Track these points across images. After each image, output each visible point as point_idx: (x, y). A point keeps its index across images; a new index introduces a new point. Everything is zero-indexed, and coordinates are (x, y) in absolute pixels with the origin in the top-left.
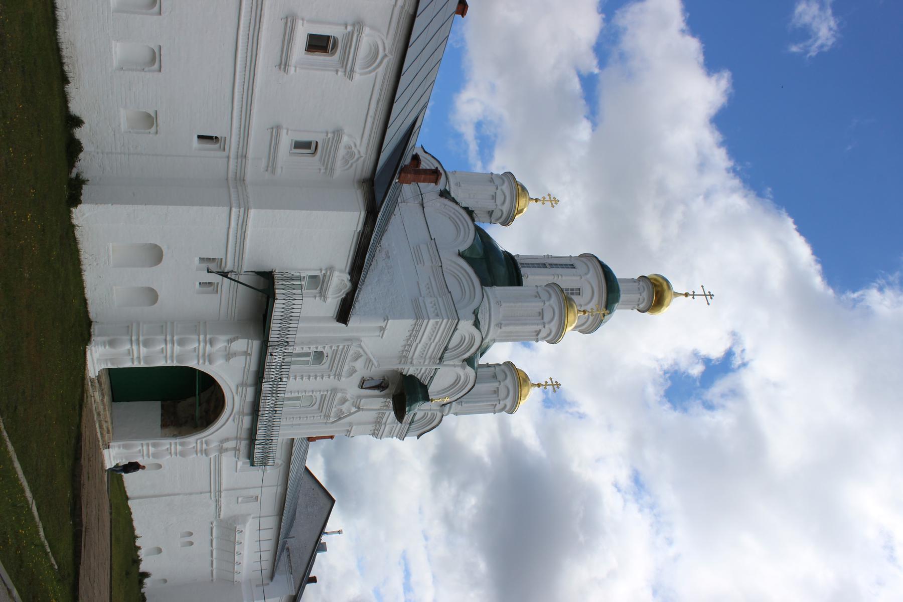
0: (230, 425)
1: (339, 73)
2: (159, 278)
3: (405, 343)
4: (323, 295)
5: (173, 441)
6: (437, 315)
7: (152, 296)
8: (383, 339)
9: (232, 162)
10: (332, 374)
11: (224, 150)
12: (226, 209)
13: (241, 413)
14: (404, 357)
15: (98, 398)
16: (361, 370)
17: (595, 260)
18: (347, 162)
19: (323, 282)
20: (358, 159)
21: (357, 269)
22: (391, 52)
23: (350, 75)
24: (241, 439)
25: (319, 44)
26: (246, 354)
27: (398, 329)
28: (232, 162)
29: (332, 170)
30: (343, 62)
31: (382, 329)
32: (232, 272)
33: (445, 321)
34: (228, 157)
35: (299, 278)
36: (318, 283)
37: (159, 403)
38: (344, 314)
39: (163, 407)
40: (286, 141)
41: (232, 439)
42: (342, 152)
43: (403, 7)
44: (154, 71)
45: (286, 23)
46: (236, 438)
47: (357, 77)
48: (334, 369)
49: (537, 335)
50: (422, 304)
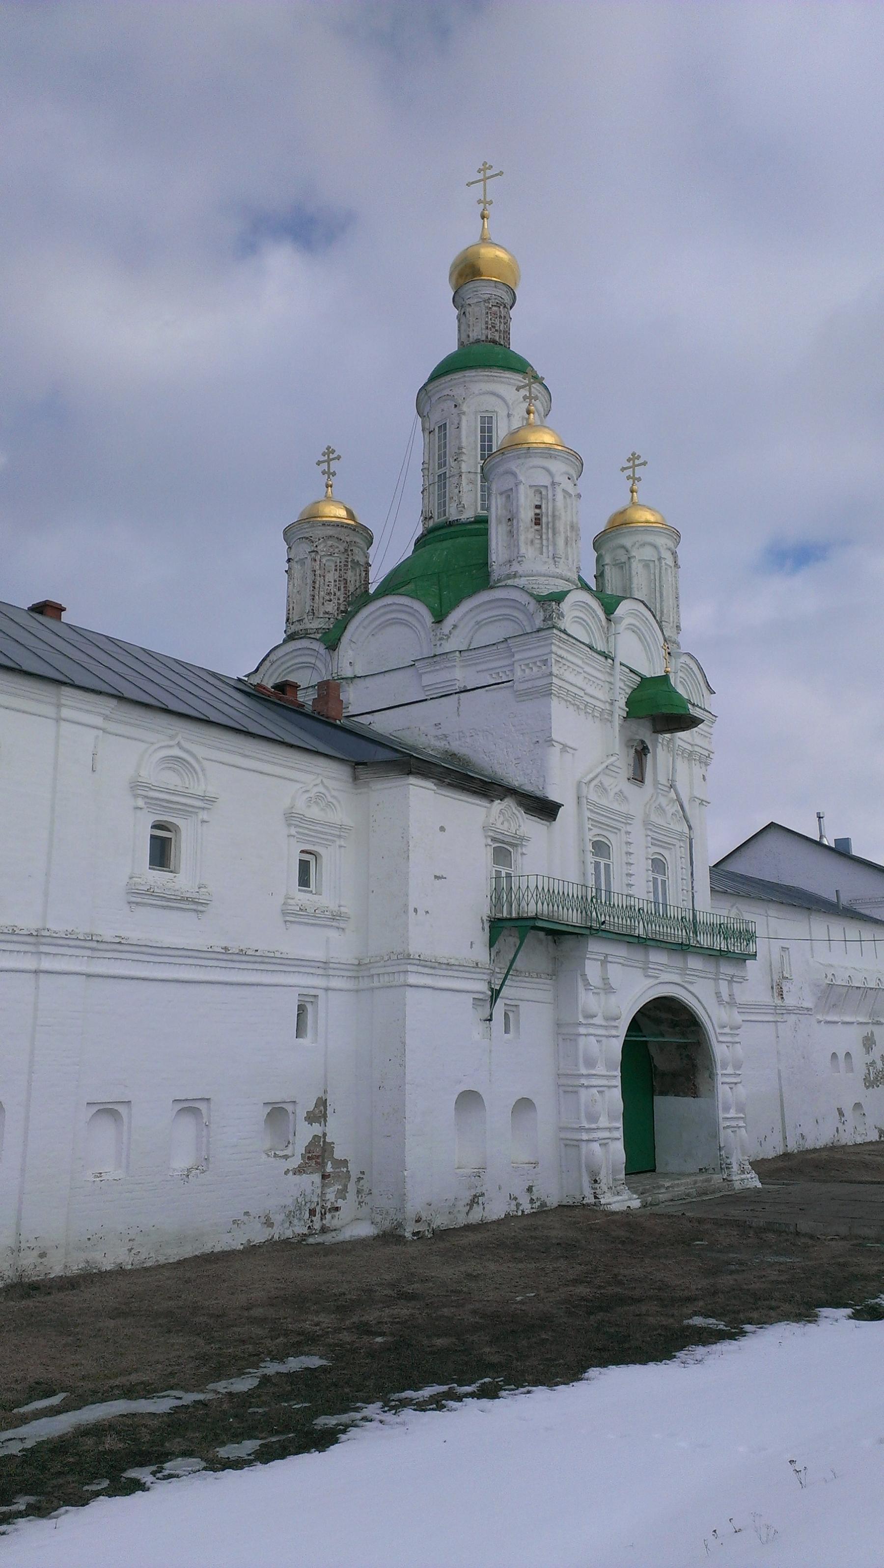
0: (699, 990)
1: (206, 818)
2: (499, 1099)
3: (582, 713)
4: (518, 842)
5: (720, 1079)
6: (545, 662)
7: (524, 1105)
8: (579, 748)
9: (335, 983)
10: (624, 828)
11: (315, 996)
12: (410, 993)
13: (683, 971)
14: (605, 717)
15: (669, 1190)
16: (620, 781)
17: (429, 388)
18: (329, 804)
19: (503, 842)
20: (326, 787)
21: (484, 786)
22: (172, 737)
23: (209, 801)
24: (717, 973)
25: (161, 852)
26: (604, 962)
27: (564, 722)
28: (335, 983)
29: (341, 827)
30: (188, 811)
31: (565, 748)
32: (490, 983)
33: (554, 648)
34: (327, 989)
35: (498, 877)
36: (503, 851)
37: (657, 1099)
38: (545, 809)
39: (663, 1093)
40: (302, 897)
41: (717, 986)
42: (315, 812)
43: (106, 718)
44: (209, 1109)
45: (137, 903)
46: (716, 980)
47: (212, 791)
48: (613, 823)
49: (570, 496)
50: (529, 685)
